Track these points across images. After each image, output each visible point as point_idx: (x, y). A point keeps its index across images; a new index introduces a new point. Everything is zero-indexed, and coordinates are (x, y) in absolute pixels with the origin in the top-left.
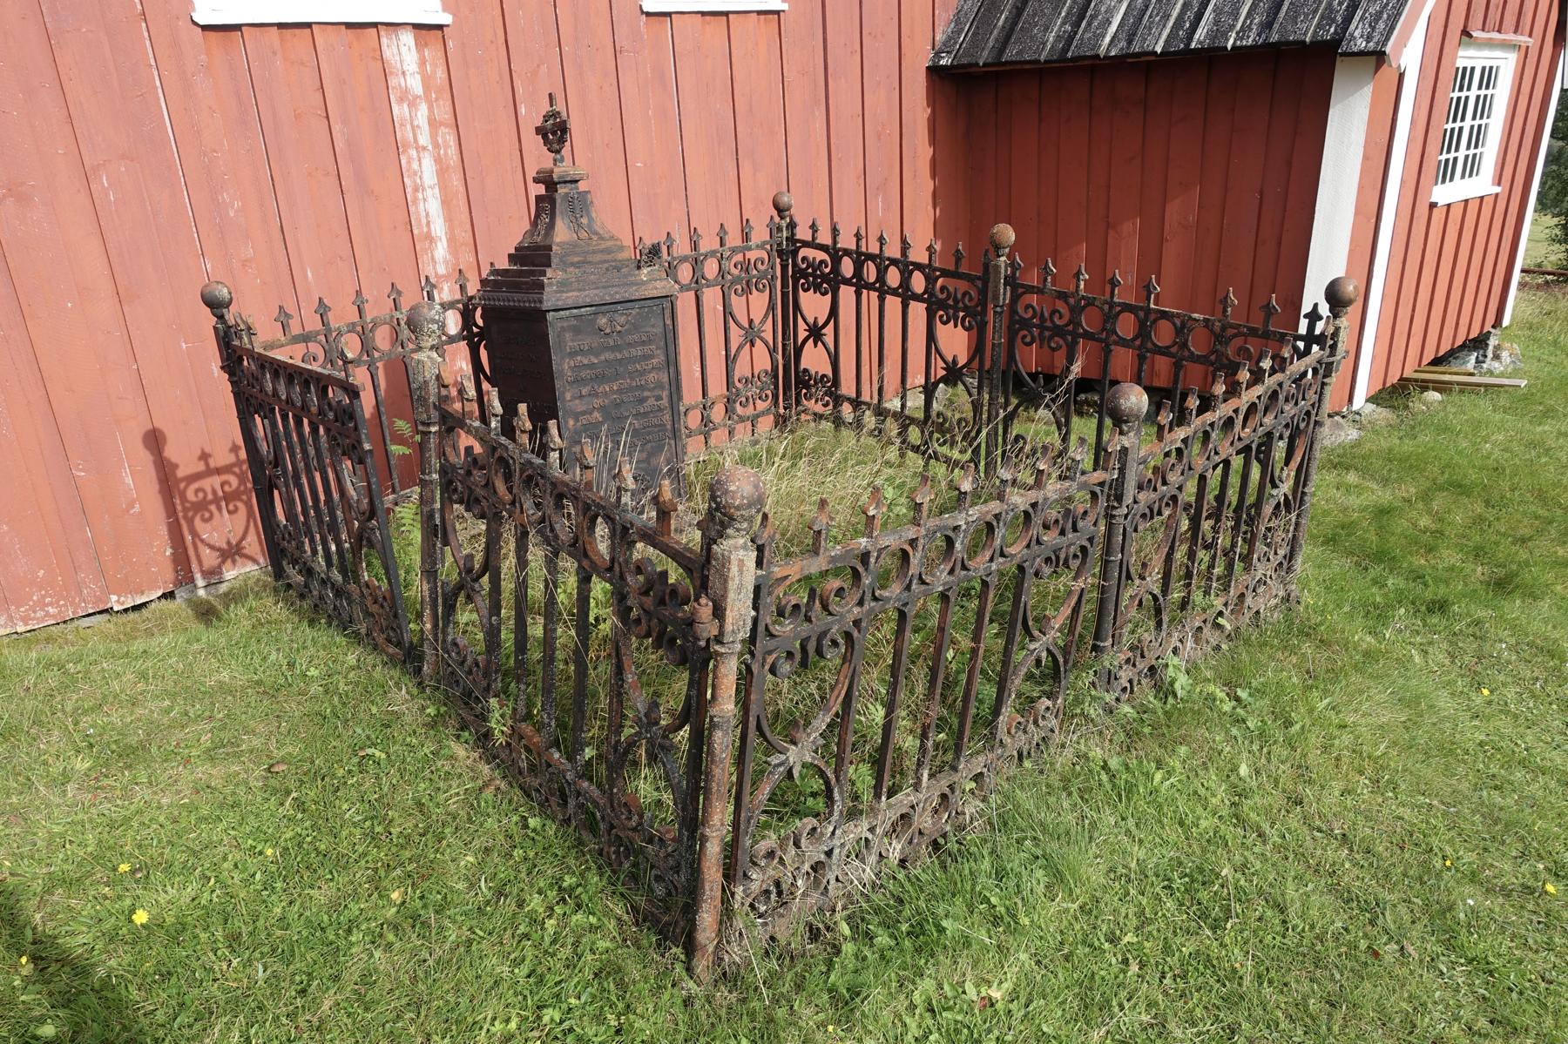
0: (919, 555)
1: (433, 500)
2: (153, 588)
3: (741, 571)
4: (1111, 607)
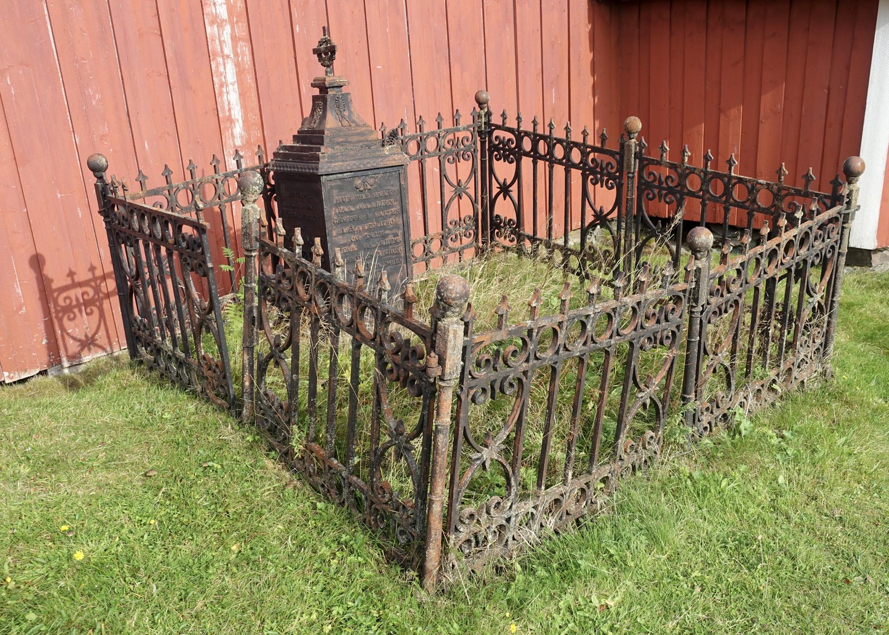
0: (564, 332)
1: (253, 301)
2: (33, 367)
3: (455, 337)
4: (693, 372)
